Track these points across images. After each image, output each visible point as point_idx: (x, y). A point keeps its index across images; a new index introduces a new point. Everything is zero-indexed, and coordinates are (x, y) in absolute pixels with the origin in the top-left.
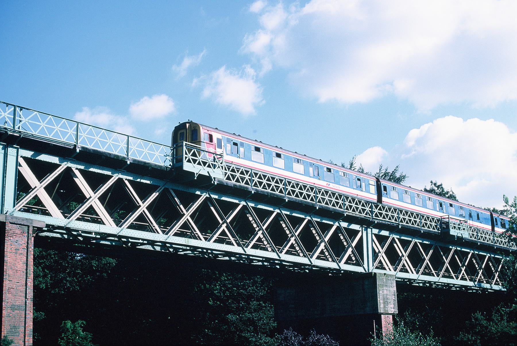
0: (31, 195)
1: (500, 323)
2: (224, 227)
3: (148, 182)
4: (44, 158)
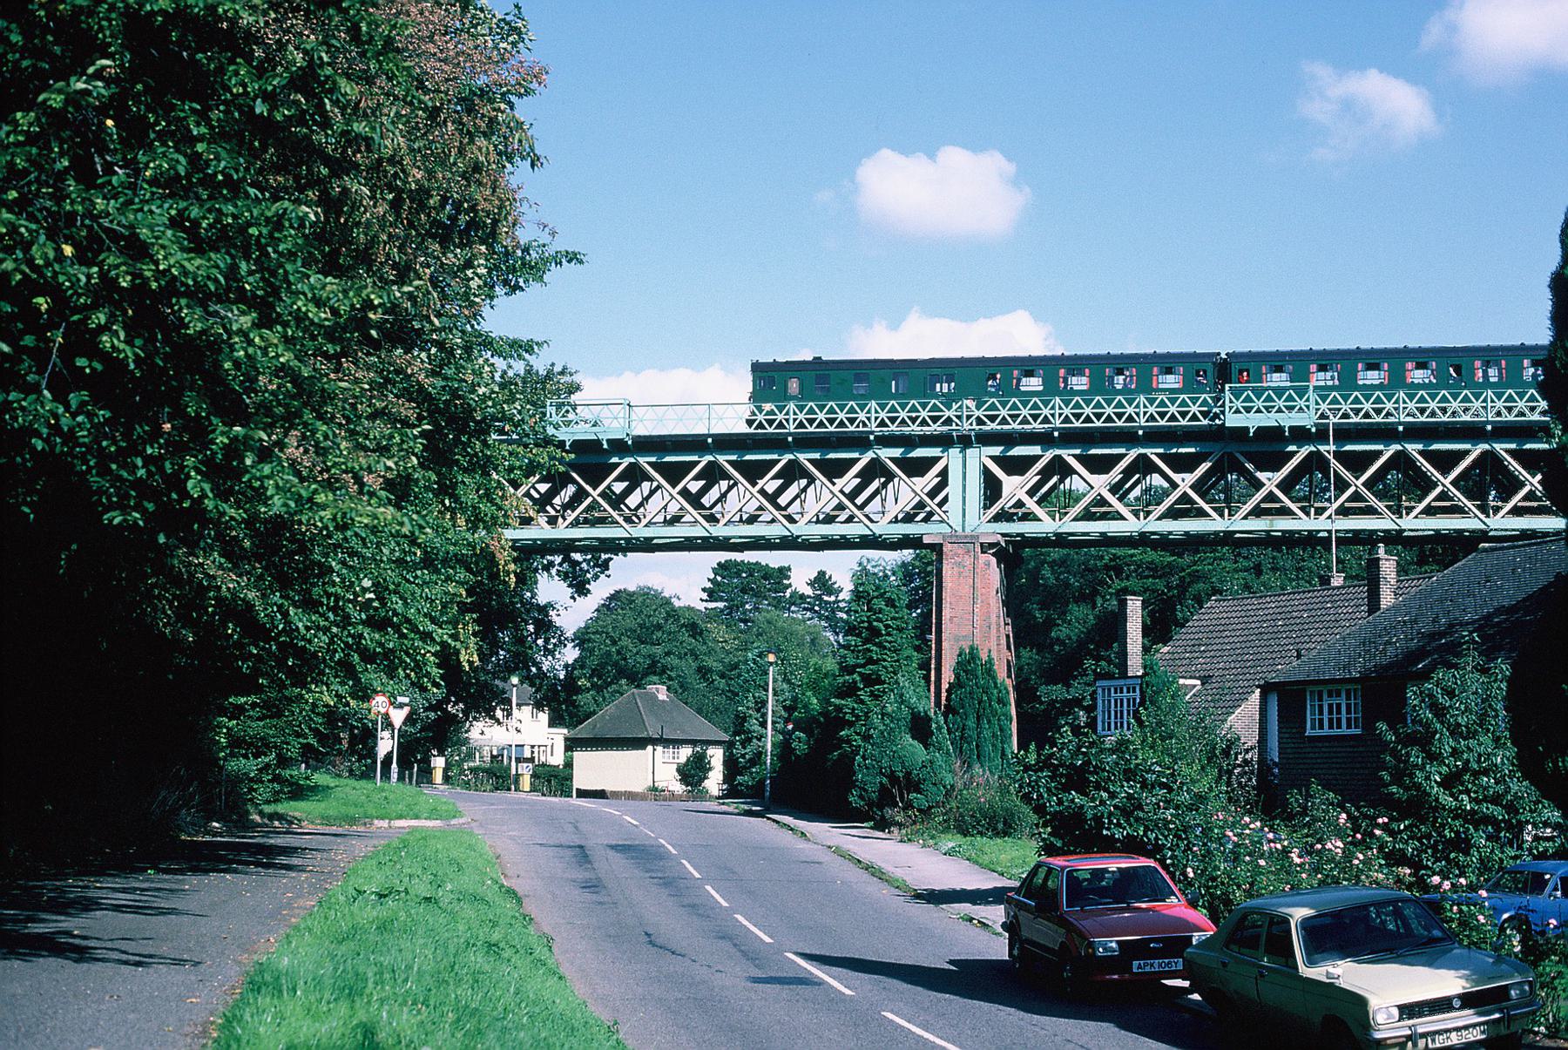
0: (600, 500)
1: (1475, 642)
2: (595, 493)
4: (1019, 451)
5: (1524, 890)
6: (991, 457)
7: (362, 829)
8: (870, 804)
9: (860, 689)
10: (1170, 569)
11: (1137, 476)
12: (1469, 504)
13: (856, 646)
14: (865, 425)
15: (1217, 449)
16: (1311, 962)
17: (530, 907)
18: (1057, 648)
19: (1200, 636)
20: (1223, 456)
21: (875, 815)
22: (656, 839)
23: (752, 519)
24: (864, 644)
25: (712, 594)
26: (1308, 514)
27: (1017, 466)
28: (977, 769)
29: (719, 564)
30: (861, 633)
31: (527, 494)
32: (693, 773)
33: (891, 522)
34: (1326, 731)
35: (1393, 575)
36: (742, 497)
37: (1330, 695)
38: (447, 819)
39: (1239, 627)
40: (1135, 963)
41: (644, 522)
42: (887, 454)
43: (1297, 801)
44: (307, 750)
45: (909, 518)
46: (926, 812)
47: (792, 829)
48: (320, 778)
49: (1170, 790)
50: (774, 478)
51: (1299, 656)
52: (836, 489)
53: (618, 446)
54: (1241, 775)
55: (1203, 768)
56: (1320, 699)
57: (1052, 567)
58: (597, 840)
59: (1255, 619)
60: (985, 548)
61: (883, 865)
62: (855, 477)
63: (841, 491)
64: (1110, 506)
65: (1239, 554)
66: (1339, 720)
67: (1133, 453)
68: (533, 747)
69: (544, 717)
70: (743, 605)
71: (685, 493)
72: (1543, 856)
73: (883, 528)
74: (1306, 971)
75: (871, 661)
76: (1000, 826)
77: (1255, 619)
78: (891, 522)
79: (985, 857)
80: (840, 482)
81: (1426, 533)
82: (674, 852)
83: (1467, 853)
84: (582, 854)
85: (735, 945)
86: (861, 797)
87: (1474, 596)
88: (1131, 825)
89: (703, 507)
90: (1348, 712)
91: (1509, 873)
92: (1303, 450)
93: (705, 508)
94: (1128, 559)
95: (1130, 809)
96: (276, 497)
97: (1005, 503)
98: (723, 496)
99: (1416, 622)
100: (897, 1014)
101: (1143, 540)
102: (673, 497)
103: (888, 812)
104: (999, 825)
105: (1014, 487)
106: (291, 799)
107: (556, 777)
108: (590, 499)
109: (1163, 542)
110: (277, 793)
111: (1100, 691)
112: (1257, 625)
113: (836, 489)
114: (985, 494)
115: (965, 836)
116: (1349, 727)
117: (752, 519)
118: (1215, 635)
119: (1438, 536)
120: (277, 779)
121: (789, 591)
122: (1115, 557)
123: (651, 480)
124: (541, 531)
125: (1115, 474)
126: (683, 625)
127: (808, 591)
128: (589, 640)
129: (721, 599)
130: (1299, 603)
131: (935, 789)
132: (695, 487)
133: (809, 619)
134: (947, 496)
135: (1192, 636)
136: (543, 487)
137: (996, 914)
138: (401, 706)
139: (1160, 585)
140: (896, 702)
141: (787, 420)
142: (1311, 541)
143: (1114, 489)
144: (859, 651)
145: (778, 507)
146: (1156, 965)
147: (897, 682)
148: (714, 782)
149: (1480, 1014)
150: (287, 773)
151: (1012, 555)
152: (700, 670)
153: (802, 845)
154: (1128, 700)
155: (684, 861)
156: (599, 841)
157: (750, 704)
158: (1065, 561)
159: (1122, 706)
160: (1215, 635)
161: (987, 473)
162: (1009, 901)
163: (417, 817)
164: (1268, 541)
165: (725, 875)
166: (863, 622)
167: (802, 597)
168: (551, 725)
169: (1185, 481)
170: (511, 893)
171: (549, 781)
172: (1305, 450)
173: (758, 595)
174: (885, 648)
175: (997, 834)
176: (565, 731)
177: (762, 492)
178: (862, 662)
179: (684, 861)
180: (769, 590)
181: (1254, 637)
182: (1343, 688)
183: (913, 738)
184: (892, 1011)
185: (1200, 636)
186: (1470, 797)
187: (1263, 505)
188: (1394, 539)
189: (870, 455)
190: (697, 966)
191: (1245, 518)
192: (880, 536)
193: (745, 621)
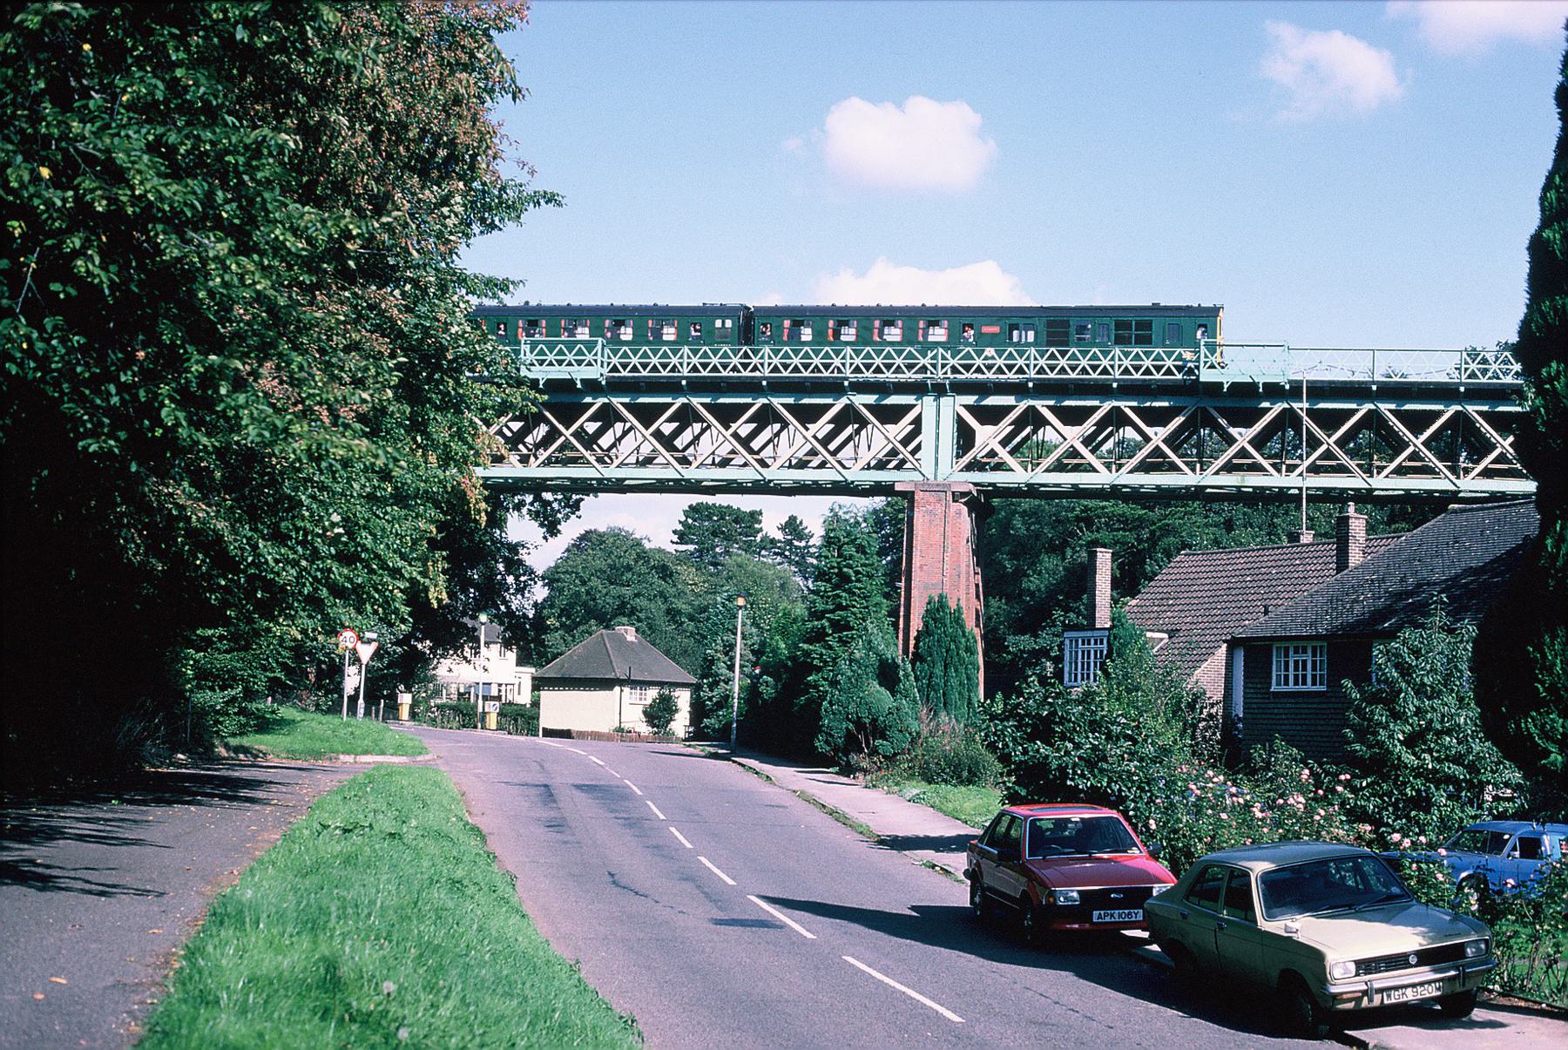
2: (568, 433)
3: (1166, 404)
5: (1483, 850)
6: (965, 406)
8: (836, 749)
9: (829, 635)
10: (1140, 523)
12: (1440, 465)
13: (825, 591)
14: (839, 371)
15: (1191, 404)
16: (1270, 916)
17: (494, 845)
19: (1169, 589)
21: (840, 760)
23: (725, 463)
25: (682, 537)
26: (1279, 471)
27: (991, 416)
28: (943, 717)
29: (690, 507)
30: (831, 578)
31: (500, 432)
32: (659, 714)
33: (863, 469)
34: (1291, 687)
35: (1363, 533)
36: (714, 440)
37: (1296, 652)
38: (413, 755)
39: (1208, 581)
40: (1096, 913)
41: (616, 462)
42: (860, 400)
43: (1260, 755)
45: (881, 465)
48: (286, 712)
51: (1266, 612)
52: (809, 435)
53: (592, 386)
54: (1206, 729)
55: (1168, 722)
56: (1287, 655)
57: (1023, 517)
58: (562, 778)
59: (1224, 574)
60: (956, 497)
61: (846, 810)
62: (829, 422)
63: (815, 437)
64: (1083, 458)
66: (1304, 677)
67: (1107, 406)
68: (500, 685)
69: (512, 656)
70: (713, 548)
71: (658, 435)
72: (1502, 816)
73: (855, 475)
75: (840, 607)
76: (965, 774)
77: (1224, 574)
78: (863, 469)
79: (950, 805)
80: (813, 427)
82: (639, 793)
83: (1427, 812)
84: (548, 794)
86: (827, 743)
88: (1095, 777)
90: (1314, 669)
91: (1467, 832)
94: (1099, 511)
95: (1094, 761)
97: (978, 451)
98: (697, 438)
99: (1383, 580)
100: (857, 958)
101: (1115, 492)
105: (987, 437)
106: (257, 732)
107: (522, 716)
108: (563, 438)
109: (1135, 496)
110: (242, 726)
111: (1067, 642)
112: (1226, 580)
113: (809, 435)
114: (958, 442)
115: (930, 783)
116: (1314, 683)
118: (1183, 589)
119: (1408, 497)
121: (760, 535)
122: (1086, 509)
123: (624, 421)
124: (512, 469)
125: (1089, 427)
126: (654, 567)
127: (779, 536)
129: (692, 542)
130: (1268, 559)
131: (901, 735)
132: (668, 429)
133: (779, 564)
135: (1160, 590)
137: (959, 862)
138: (369, 641)
139: (1131, 538)
140: (864, 648)
142: (1282, 498)
143: (1087, 441)
145: (751, 451)
146: (1117, 915)
147: (865, 629)
148: (680, 724)
149: (1435, 971)
150: (253, 706)
151: (983, 504)
152: (668, 612)
154: (1096, 652)
155: (649, 803)
158: (1035, 513)
159: (1089, 658)
161: (961, 422)
162: (972, 849)
163: (383, 753)
166: (833, 568)
167: (773, 541)
169: (1158, 435)
171: (516, 720)
172: (1279, 407)
173: (728, 538)
174: (854, 593)
175: (961, 783)
176: (533, 670)
177: (736, 435)
179: (649, 803)
180: (740, 534)
183: (880, 685)
184: (852, 955)
185: (1169, 589)
187: (1235, 461)
188: (1364, 498)
189: (844, 401)
191: (1217, 473)
193: (715, 565)
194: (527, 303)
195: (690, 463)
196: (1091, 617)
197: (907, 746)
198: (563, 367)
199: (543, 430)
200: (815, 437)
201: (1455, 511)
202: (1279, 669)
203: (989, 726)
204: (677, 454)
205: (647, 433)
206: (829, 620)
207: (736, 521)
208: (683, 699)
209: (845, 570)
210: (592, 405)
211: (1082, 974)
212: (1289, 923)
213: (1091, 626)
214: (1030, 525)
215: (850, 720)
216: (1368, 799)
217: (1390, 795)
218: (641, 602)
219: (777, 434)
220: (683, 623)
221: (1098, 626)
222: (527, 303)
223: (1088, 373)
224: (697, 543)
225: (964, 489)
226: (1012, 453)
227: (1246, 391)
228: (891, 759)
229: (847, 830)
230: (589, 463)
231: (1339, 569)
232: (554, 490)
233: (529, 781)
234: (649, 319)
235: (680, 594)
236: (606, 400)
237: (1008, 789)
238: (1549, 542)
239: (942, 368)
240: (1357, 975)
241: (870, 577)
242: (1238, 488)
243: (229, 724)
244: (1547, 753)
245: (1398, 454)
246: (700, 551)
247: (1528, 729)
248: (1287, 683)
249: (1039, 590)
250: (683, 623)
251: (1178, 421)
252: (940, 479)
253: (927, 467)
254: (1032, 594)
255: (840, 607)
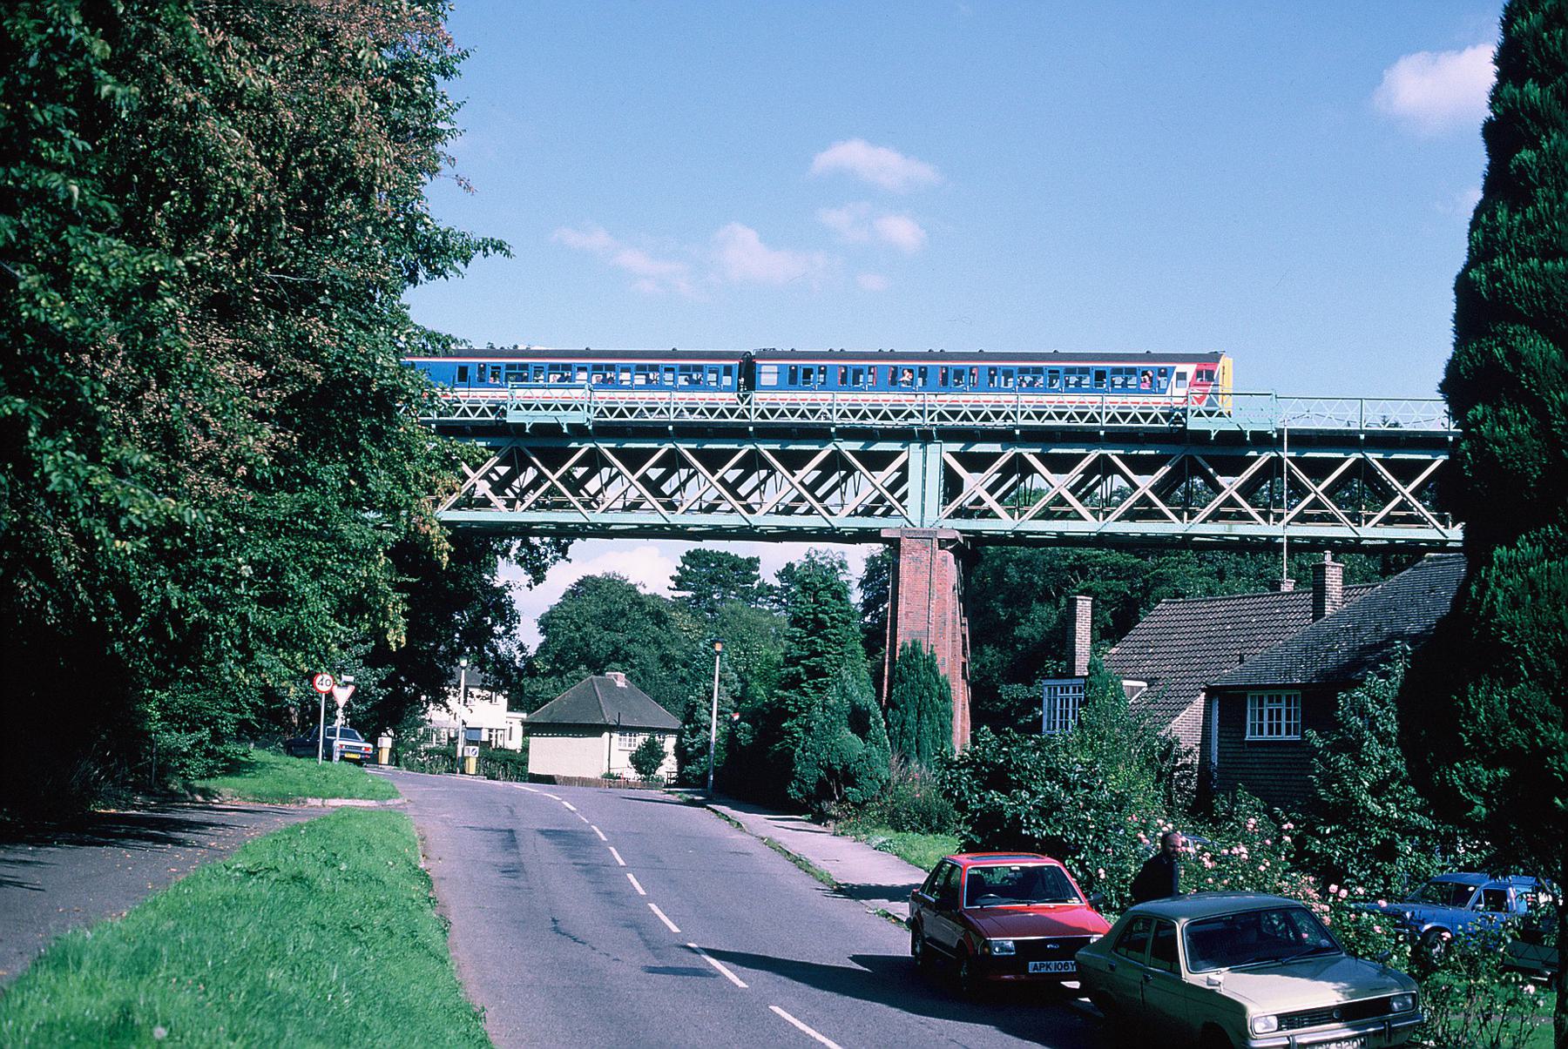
0: (558, 484)
2: (554, 478)
3: (1153, 452)
4: (979, 448)
5: (1446, 902)
6: (952, 453)
7: (293, 807)
8: (809, 796)
9: (804, 682)
10: (1134, 572)
11: (1098, 477)
12: (1428, 514)
13: (801, 637)
14: (744, 417)
15: (1178, 452)
16: (1194, 968)
17: (442, 891)
18: (1019, 647)
19: (1149, 637)
20: (1182, 461)
21: (812, 807)
22: (589, 825)
23: (712, 508)
24: (809, 636)
25: (680, 583)
26: (1267, 520)
27: (977, 463)
28: (914, 765)
29: (688, 553)
30: (807, 624)
31: (486, 477)
32: (646, 760)
33: (850, 515)
34: (1266, 736)
35: (1339, 582)
36: (701, 487)
37: (1271, 701)
38: (383, 798)
39: (1188, 630)
40: (1031, 964)
41: (603, 507)
42: (846, 447)
43: (1222, 805)
44: (243, 725)
45: (869, 512)
46: (860, 806)
47: (729, 820)
48: (257, 754)
49: (1092, 789)
50: (734, 467)
51: (1241, 661)
52: (795, 481)
53: (579, 431)
54: (1181, 778)
55: (1141, 770)
56: (1261, 704)
57: (1017, 565)
58: (529, 823)
59: (1204, 622)
60: (943, 544)
61: (809, 857)
62: (816, 469)
63: (801, 483)
64: (1070, 506)
65: (1204, 558)
66: (1279, 726)
67: (1094, 454)
68: (491, 730)
69: (502, 702)
70: (710, 594)
71: (645, 480)
72: (1469, 868)
73: (841, 521)
74: (1189, 977)
75: (815, 653)
76: (935, 822)
77: (1204, 622)
78: (850, 515)
79: (915, 854)
80: (800, 474)
81: (1379, 542)
82: (604, 839)
83: (1392, 861)
84: (510, 839)
85: (640, 934)
86: (799, 789)
87: (1418, 605)
88: (1050, 826)
89: (663, 495)
90: (1288, 718)
91: (1434, 884)
92: (1264, 455)
93: (665, 496)
94: (1092, 559)
95: (1049, 808)
96: (54, 474)
97: (964, 500)
98: (683, 485)
99: (1358, 629)
100: (785, 1009)
101: (1102, 540)
102: (632, 484)
103: (825, 805)
104: (930, 822)
105: (975, 484)
106: (226, 774)
107: (512, 761)
108: (549, 483)
109: (1040, 542)
110: (210, 769)
111: (1046, 690)
112: (1206, 628)
113: (795, 481)
114: (945, 490)
115: (898, 831)
116: (1288, 733)
117: (712, 508)
118: (1164, 637)
119: (1392, 546)
120: (209, 754)
121: (757, 582)
122: (1079, 557)
123: (611, 466)
124: (499, 513)
125: (1076, 474)
126: (649, 613)
127: (777, 583)
128: (554, 625)
129: (689, 588)
130: (1248, 607)
131: (870, 783)
132: (655, 474)
133: (776, 611)
134: (906, 493)
135: (1141, 638)
136: (503, 470)
137: (903, 909)
138: (347, 684)
139: (1124, 587)
140: (838, 694)
141: (749, 410)
142: (1269, 546)
143: (1073, 490)
144: (804, 643)
145: (738, 497)
146: (1053, 966)
147: (839, 675)
148: (668, 767)
149: (1353, 1028)
150: (220, 749)
151: (970, 551)
152: (662, 658)
153: (736, 836)
154: (1074, 700)
155: (612, 849)
156: (530, 826)
157: (701, 694)
158: (1029, 562)
159: (1067, 706)
160: (1164, 637)
161: (947, 469)
162: (915, 898)
163: (351, 797)
164: (1223, 544)
165: (650, 864)
166: (809, 613)
167: (770, 588)
168: (509, 710)
169: (1145, 483)
170: (424, 876)
171: (505, 766)
172: (1266, 456)
173: (725, 585)
174: (829, 640)
175: (931, 831)
176: (524, 715)
177: (722, 481)
178: (807, 653)
179: (612, 849)
180: (738, 581)
181: (1202, 641)
182: (1284, 694)
183: (853, 732)
184: (781, 1006)
185: (1149, 637)
186: (1398, 807)
187: (1222, 509)
188: (1342, 548)
189: (830, 447)
190: (594, 954)
191: (1204, 521)
192: (839, 529)
193: (712, 611)
194: (516, 347)
195: (676, 509)
196: (1072, 666)
197: (877, 793)
198: (550, 412)
199: (530, 475)
200: (801, 483)
201: (1430, 559)
202: (1253, 718)
203: (944, 774)
204: (665, 500)
205: (633, 478)
206: (804, 666)
207: (734, 568)
208: (670, 743)
209: (820, 615)
210: (578, 450)
211: (1007, 1029)
212: (1213, 976)
213: (1070, 673)
214: (1024, 572)
215: (821, 767)
216: (1334, 848)
217: (1353, 844)
218: (635, 648)
219: (764, 482)
220: (676, 669)
221: (1077, 674)
222: (516, 347)
223: (467, 415)
224: (694, 590)
225: (950, 536)
226: (1000, 500)
227: (1233, 439)
228: (860, 806)
229: (808, 879)
230: (575, 508)
231: (1315, 618)
232: (541, 534)
233: (495, 826)
234: (650, 365)
235: (674, 640)
236: (672, 446)
237: (964, 837)
238: (1474, 588)
239: (929, 415)
240: (1280, 1029)
241: (847, 623)
242: (1220, 536)
243: (196, 765)
244: (1472, 805)
245: (1385, 504)
246: (697, 598)
247: (1452, 781)
248: (1261, 732)
249: (1033, 638)
250: (676, 669)
251: (1164, 470)
252: (926, 526)
253: (914, 514)
254: (1026, 641)
255: (815, 653)
